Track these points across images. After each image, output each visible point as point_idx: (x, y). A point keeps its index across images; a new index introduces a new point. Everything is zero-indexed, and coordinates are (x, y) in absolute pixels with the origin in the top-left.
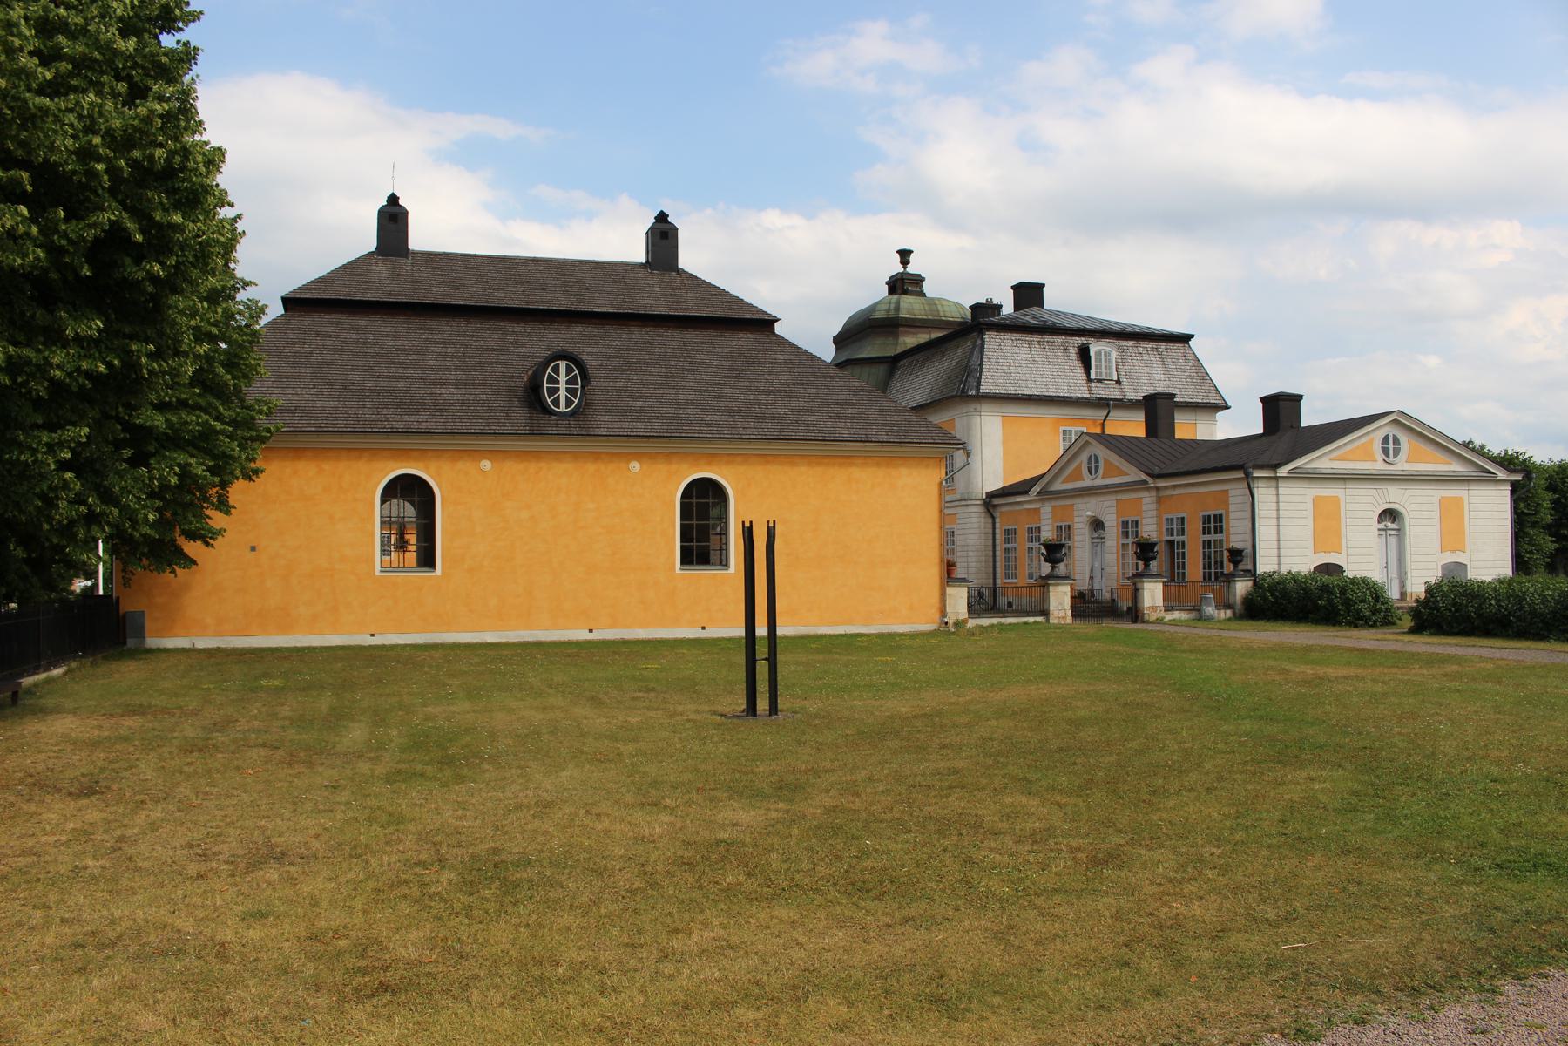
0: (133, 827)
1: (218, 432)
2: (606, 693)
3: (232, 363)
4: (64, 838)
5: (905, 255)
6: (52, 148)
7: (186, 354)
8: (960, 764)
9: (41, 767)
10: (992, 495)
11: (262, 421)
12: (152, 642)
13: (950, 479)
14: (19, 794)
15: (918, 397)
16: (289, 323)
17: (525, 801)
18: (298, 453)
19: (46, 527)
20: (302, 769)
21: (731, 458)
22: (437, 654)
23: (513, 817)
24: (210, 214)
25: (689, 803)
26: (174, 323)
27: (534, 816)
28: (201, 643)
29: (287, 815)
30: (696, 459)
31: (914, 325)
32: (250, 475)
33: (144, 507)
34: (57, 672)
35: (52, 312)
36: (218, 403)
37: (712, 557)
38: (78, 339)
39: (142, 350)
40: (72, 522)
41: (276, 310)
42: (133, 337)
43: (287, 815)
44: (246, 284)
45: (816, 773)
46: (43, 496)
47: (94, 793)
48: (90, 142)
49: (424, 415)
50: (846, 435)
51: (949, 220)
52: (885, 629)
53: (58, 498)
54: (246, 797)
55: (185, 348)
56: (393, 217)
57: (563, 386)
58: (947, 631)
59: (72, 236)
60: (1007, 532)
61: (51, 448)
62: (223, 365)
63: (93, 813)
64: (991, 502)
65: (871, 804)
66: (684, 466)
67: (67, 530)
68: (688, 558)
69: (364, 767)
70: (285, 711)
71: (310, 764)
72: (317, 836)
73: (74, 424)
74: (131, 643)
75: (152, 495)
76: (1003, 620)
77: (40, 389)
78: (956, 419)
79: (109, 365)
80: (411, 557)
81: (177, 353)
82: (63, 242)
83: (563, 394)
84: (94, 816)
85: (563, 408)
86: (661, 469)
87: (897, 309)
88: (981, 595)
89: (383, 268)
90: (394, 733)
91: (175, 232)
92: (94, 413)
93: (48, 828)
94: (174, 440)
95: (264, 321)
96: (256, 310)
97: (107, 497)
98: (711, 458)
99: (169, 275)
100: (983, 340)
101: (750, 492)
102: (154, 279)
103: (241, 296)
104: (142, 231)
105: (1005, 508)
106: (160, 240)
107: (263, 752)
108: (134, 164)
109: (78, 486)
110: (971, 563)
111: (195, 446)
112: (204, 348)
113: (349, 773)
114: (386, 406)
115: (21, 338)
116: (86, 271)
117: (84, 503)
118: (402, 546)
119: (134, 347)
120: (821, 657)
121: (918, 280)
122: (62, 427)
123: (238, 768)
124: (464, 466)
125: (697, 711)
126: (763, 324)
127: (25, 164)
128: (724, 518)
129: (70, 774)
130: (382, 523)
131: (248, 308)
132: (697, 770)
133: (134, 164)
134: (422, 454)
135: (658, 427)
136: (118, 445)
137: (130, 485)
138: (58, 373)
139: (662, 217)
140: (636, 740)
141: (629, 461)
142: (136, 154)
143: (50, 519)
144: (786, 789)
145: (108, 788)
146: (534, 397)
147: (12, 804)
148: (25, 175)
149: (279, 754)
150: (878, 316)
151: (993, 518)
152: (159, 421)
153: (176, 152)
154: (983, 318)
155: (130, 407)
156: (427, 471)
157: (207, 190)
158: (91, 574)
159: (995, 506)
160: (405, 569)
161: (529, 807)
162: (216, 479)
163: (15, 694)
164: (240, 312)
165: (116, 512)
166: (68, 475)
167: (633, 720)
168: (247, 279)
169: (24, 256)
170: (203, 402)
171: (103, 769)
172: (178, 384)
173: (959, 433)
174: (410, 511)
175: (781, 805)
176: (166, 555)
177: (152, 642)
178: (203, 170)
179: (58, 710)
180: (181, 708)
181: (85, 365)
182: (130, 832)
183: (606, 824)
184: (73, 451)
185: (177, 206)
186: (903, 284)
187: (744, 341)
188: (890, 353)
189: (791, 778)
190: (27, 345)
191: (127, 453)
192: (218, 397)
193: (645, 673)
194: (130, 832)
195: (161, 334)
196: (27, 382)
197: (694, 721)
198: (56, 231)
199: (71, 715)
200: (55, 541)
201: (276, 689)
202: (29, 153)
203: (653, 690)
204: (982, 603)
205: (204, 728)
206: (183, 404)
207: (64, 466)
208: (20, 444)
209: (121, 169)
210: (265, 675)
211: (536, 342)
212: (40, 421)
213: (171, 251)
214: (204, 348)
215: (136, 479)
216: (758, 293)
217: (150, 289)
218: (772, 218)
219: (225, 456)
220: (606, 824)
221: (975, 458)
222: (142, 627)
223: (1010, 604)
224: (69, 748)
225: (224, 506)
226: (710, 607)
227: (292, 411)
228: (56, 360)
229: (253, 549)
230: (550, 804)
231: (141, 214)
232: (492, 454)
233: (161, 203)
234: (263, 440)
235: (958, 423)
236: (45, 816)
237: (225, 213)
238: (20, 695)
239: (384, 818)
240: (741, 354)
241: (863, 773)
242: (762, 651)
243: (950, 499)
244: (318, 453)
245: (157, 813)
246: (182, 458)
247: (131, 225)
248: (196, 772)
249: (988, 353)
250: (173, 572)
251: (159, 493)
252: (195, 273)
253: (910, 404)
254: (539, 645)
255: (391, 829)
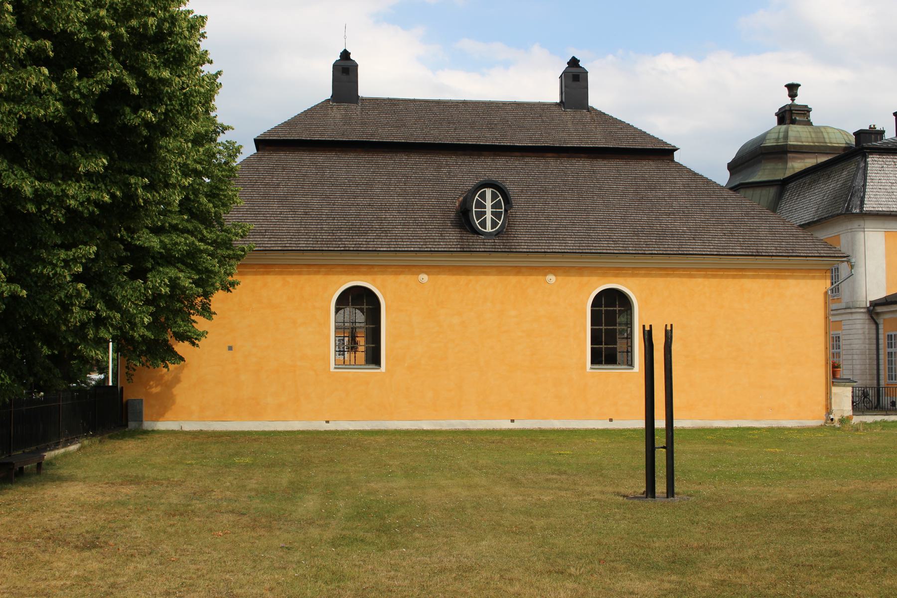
0: (123, 576)
1: (201, 251)
2: (524, 475)
3: (213, 194)
4: (68, 583)
5: (793, 89)
6: (68, 20)
7: (174, 186)
8: (841, 547)
9: (55, 524)
10: (875, 304)
11: (238, 242)
12: (147, 425)
13: (835, 290)
14: (37, 545)
15: (807, 216)
16: (260, 160)
17: (448, 565)
18: (267, 268)
19: (64, 328)
20: (262, 532)
21: (634, 272)
22: (381, 439)
23: (437, 579)
24: (194, 69)
25: (592, 572)
26: (164, 161)
27: (455, 579)
28: (188, 427)
29: (248, 570)
30: (605, 272)
31: (801, 151)
32: (228, 287)
33: (140, 313)
34: (73, 448)
35: (68, 153)
36: (202, 227)
37: (619, 356)
38: (89, 175)
39: (138, 182)
40: (84, 325)
41: (249, 150)
42: (131, 173)
43: (248, 570)
44: (225, 129)
45: (707, 550)
46: (61, 303)
47: (95, 547)
48: (97, 15)
49: (371, 236)
50: (738, 250)
51: (829, 56)
52: (775, 424)
53: (73, 305)
54: (215, 555)
55: (173, 180)
56: (345, 69)
57: (489, 210)
58: (832, 427)
59: (84, 91)
60: (890, 337)
61: (67, 263)
62: (207, 196)
63: (93, 563)
64: (874, 310)
65: (757, 580)
66: (594, 279)
67: (80, 331)
68: (597, 359)
69: (314, 532)
70: (252, 484)
71: (270, 528)
72: (271, 589)
73: (86, 244)
74: (132, 425)
75: (148, 302)
76: (886, 418)
77: (60, 216)
78: (840, 235)
79: (113, 196)
80: (361, 356)
81: (167, 185)
82: (77, 96)
83: (489, 216)
84: (94, 565)
85: (489, 229)
86: (574, 281)
87: (786, 137)
88: (865, 395)
89: (337, 112)
90: (341, 504)
91: (164, 85)
92: (101, 235)
93: (57, 574)
94: (167, 258)
95: (240, 159)
96: (233, 150)
97: (112, 304)
98: (618, 272)
99: (160, 122)
100: (866, 163)
101: (654, 300)
102: (147, 124)
103: (221, 138)
104: (139, 85)
105: (888, 315)
106: (153, 93)
107: (232, 517)
108: (132, 31)
109: (88, 295)
110: (856, 363)
111: (184, 263)
112: (187, 181)
113: (302, 537)
114: (340, 229)
115: (45, 175)
116: (95, 120)
117: (93, 308)
118: (353, 348)
119: (133, 181)
120: (716, 447)
121: (805, 111)
122: (76, 246)
123: (210, 530)
124: (405, 279)
125: (602, 493)
126: (665, 153)
127: (47, 34)
128: (630, 324)
129: (77, 530)
130: (337, 328)
131: (227, 148)
132: (600, 544)
133: (132, 31)
134: (369, 269)
135: (571, 245)
136: (121, 262)
137: (129, 293)
138: (72, 202)
139: (574, 62)
140: (547, 516)
141: (546, 275)
142: (134, 23)
143: (66, 322)
144: (679, 563)
145: (106, 543)
146: (464, 220)
147: (32, 554)
148: (48, 44)
149: (245, 520)
150: (768, 144)
151: (877, 324)
152: (154, 242)
153: (165, 20)
154: (868, 143)
155: (131, 231)
156: (374, 282)
157: (190, 50)
158: (103, 370)
159: (878, 314)
160: (355, 365)
161: (451, 571)
162: (200, 290)
163: (39, 465)
164: (220, 152)
165: (118, 316)
166: (81, 286)
167: (546, 498)
168: (226, 124)
169: (46, 108)
170: (190, 226)
171: (103, 528)
172: (170, 212)
173: (844, 247)
174: (360, 317)
175: (674, 578)
176: (159, 351)
177: (147, 425)
178: (187, 33)
179: (71, 479)
180: (168, 479)
181: (94, 196)
182: (120, 580)
183: (517, 587)
184: (85, 266)
185: (166, 64)
186: (787, 116)
187: (647, 168)
188: (780, 176)
189: (684, 553)
190: (50, 180)
191: (128, 268)
192: (202, 223)
193: (559, 458)
194: (120, 580)
195: (155, 170)
196: (48, 210)
197: (599, 501)
198: (72, 87)
199: (82, 480)
200: (70, 340)
201: (246, 465)
202: (50, 25)
203: (565, 473)
204: (866, 402)
205: (185, 496)
206: (174, 228)
207: (77, 278)
208: (43, 260)
209: (122, 36)
210: (237, 454)
211: (466, 172)
212: (59, 242)
213: (161, 101)
214: (187, 181)
215: (134, 290)
216: (659, 127)
217: (145, 133)
218: (667, 62)
219: (208, 271)
220: (517, 587)
221: (860, 270)
222: (141, 412)
223: (893, 404)
224: (78, 509)
225: (206, 311)
226: (613, 402)
227: (262, 234)
228: (71, 192)
229: (230, 348)
230: (470, 569)
231: (137, 71)
232: (429, 269)
233: (154, 63)
234: (238, 258)
235: (844, 240)
236: (55, 564)
237: (207, 69)
238: (44, 466)
239: (328, 576)
240: (644, 179)
241: (750, 551)
242: (660, 440)
243: (836, 305)
244: (284, 268)
245: (143, 566)
246: (172, 272)
247: (129, 81)
248: (176, 532)
249: (871, 173)
250: (166, 366)
251: (154, 300)
252: (181, 119)
253: (799, 222)
254: (468, 432)
255: (333, 586)
